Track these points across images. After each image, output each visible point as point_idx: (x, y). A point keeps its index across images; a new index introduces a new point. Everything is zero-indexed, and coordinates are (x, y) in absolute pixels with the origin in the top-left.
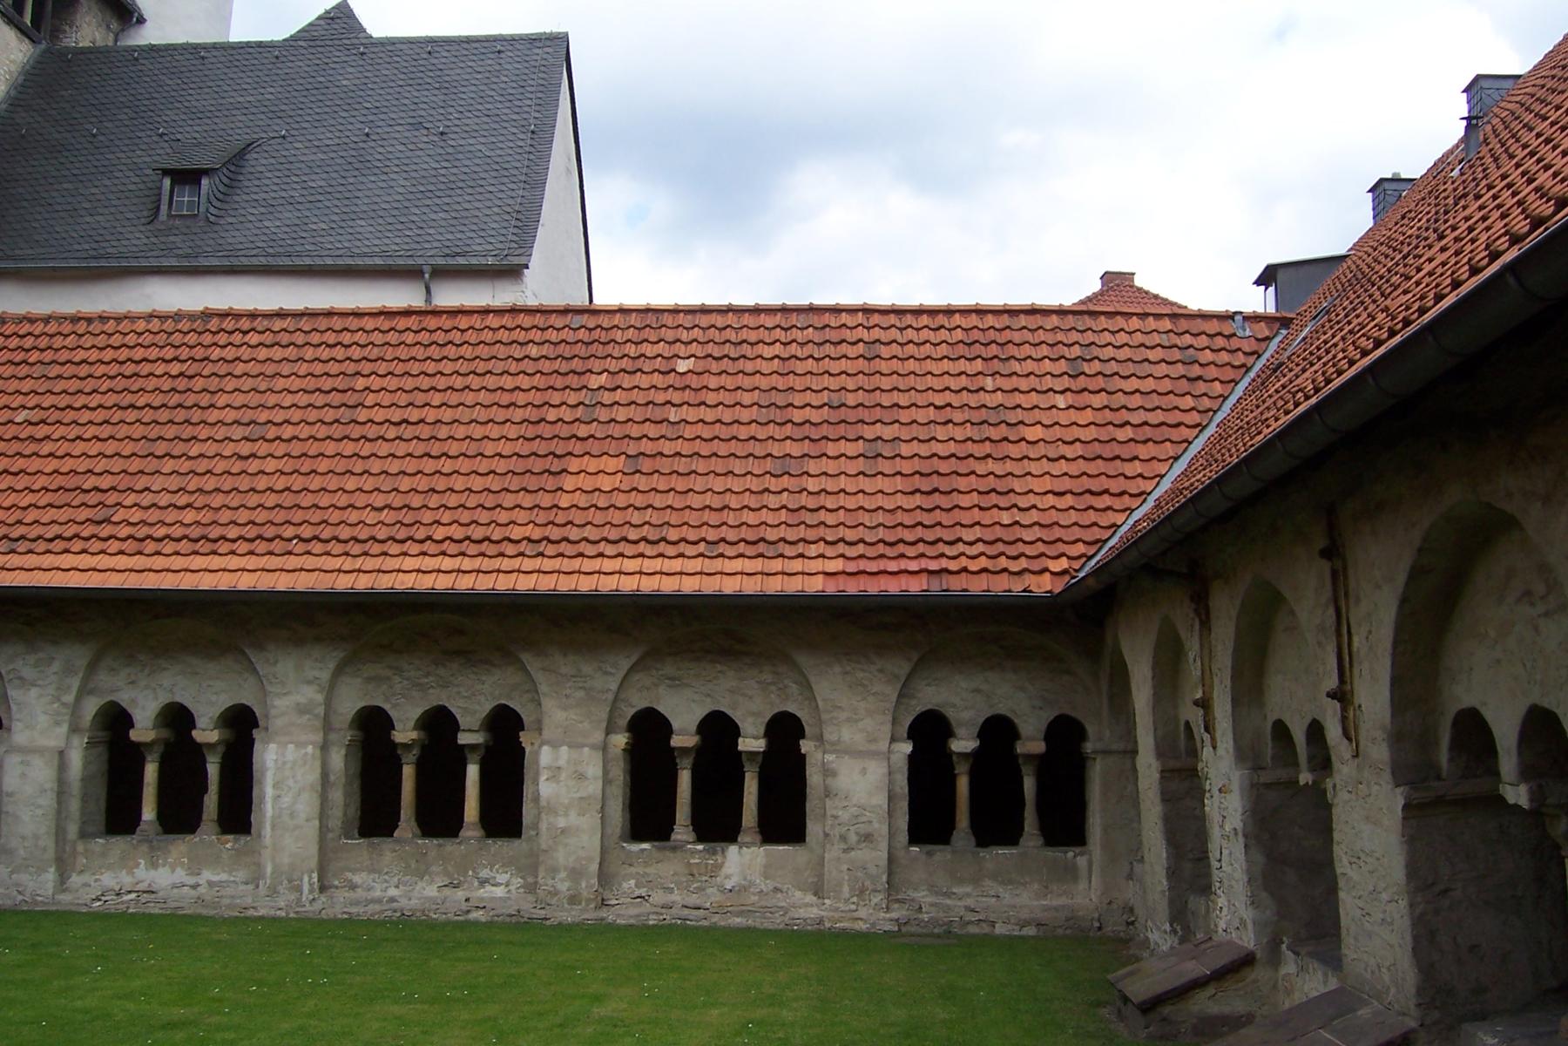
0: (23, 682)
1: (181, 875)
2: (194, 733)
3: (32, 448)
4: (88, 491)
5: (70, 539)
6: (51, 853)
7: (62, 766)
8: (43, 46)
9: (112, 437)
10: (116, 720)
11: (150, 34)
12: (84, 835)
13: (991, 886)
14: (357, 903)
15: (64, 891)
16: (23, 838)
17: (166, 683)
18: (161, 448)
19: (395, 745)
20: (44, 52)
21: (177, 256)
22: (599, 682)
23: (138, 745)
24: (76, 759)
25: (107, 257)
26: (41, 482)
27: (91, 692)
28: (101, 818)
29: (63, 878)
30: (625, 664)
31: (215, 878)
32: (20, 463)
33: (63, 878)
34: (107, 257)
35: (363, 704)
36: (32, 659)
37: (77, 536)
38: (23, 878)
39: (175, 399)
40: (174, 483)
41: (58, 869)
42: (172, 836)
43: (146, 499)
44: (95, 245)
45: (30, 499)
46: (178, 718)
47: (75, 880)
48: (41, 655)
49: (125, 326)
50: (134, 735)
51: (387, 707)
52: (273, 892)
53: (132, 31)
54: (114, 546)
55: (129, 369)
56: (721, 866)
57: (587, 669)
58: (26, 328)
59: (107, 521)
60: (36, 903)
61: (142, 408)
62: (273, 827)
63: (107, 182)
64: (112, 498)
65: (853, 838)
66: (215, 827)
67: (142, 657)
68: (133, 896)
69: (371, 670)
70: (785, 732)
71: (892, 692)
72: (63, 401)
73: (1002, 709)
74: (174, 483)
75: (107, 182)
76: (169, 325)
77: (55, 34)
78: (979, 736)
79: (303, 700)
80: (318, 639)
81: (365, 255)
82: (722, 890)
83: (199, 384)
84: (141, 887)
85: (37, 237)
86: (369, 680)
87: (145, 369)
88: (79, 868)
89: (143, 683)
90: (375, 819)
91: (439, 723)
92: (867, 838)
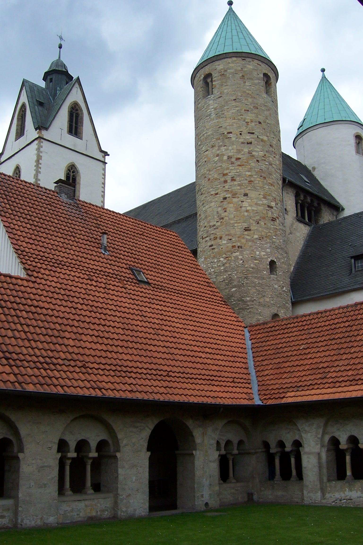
0: (306, 432)
2: (359, 445)
3: (305, 356)
4: (321, 368)
5: (358, 380)
6: (319, 486)
7: (320, 458)
8: (313, 226)
9: (328, 350)
10: (335, 442)
11: (347, 213)
12: (329, 480)
15: (324, 499)
16: (310, 482)
18: (342, 351)
20: (313, 228)
21: (359, 284)
23: (273, 454)
24: (324, 455)
25: (338, 288)
26: (307, 367)
27: (327, 433)
28: (335, 475)
29: (323, 495)
32: (302, 362)
33: (323, 495)
34: (338, 288)
37: (316, 384)
38: (311, 495)
39: (347, 334)
40: (346, 362)
41: (321, 492)
42: (356, 480)
43: (337, 369)
44: (334, 286)
45: (304, 373)
47: (327, 495)
49: (332, 313)
50: (341, 447)
53: (341, 214)
54: (327, 385)
55: (334, 326)
58: (304, 318)
59: (325, 377)
60: (315, 503)
61: (337, 339)
63: (336, 265)
64: (327, 370)
66: (70, 493)
68: (345, 501)
72: (315, 340)
74: (346, 362)
75: (336, 265)
76: (345, 310)
77: (316, 221)
78: (148, 450)
83: (354, 328)
84: (348, 497)
85: (317, 287)
87: (338, 326)
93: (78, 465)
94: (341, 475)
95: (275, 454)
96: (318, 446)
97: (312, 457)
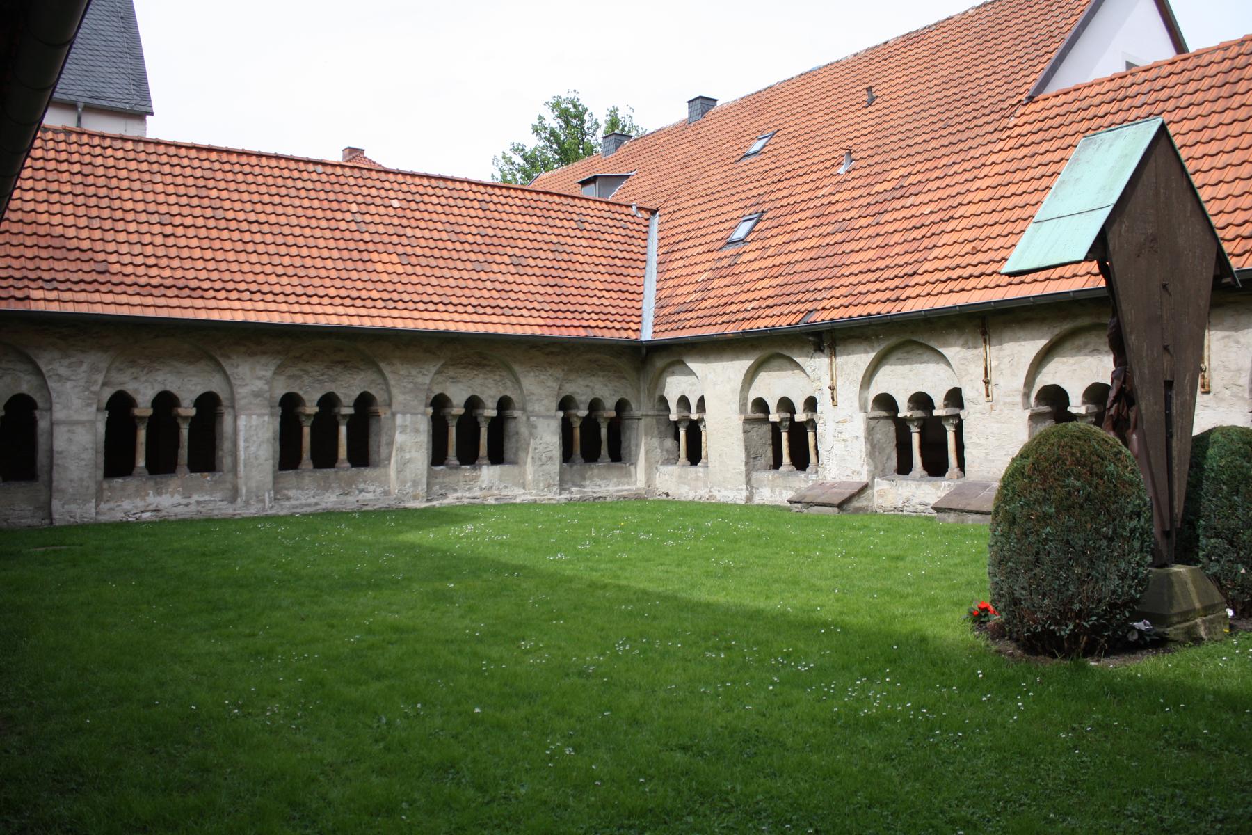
0: (60, 378)
1: (178, 498)
10: (886, 402)
14: (297, 507)
16: (71, 481)
17: (159, 379)
22: (420, 379)
25: (105, 99)
30: (434, 370)
31: (201, 499)
35: (284, 392)
36: (66, 362)
38: (73, 507)
46: (166, 402)
48: (73, 360)
51: (301, 393)
52: (247, 504)
57: (414, 372)
62: (245, 465)
66: (486, 461)
67: (142, 362)
69: (294, 371)
70: (365, 402)
71: (555, 385)
73: (598, 395)
80: (264, 353)
82: (481, 489)
84: (151, 508)
86: (290, 377)
88: (105, 498)
89: (143, 379)
90: (904, 467)
91: (329, 402)
93: (590, 424)
94: (904, 467)
95: (142, 418)
96: (89, 409)
97: (80, 430)
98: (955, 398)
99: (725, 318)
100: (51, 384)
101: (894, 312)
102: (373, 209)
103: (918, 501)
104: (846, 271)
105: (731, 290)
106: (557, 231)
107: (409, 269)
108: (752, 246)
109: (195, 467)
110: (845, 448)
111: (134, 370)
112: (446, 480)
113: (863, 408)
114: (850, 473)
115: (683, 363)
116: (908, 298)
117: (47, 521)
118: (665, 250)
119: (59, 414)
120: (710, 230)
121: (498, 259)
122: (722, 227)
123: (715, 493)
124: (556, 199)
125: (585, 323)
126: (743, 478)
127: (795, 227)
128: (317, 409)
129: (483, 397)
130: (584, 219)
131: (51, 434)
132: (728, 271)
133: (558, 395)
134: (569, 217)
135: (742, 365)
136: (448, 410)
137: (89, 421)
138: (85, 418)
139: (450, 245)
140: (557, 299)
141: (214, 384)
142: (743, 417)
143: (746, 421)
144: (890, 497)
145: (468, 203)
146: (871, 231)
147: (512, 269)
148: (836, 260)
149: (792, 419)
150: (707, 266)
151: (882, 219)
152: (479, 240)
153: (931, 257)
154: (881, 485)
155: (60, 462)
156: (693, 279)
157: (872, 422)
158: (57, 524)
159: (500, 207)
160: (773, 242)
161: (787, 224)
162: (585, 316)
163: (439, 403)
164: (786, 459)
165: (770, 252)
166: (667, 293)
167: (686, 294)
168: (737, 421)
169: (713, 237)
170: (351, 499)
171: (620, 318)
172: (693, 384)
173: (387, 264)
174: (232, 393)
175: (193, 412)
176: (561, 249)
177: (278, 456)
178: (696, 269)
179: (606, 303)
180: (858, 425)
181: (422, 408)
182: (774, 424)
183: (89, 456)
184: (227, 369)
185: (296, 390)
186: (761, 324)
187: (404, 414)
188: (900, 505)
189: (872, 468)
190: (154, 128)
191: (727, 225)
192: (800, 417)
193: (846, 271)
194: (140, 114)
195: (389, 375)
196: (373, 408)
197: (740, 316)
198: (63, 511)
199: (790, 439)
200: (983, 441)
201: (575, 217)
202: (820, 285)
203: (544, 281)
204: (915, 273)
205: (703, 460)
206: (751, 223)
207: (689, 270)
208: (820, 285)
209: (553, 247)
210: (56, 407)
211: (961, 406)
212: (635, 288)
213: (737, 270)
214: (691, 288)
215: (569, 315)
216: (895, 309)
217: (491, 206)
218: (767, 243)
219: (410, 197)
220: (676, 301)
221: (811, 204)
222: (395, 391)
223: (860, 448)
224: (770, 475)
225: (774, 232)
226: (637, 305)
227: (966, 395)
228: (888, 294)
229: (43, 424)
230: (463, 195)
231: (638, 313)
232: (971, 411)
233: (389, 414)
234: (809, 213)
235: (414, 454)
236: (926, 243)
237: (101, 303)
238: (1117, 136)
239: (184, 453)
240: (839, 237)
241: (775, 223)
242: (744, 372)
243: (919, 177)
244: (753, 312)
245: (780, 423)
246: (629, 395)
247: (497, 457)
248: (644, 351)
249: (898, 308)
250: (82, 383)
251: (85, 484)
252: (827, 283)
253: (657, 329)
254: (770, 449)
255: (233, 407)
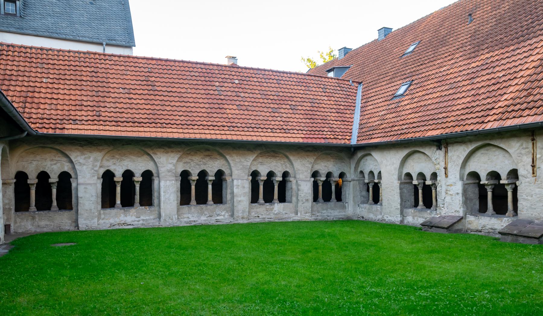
1: (134, 218)
10: (475, 175)
13: (330, 211)
16: (87, 210)
19: (133, 181)
22: (245, 164)
30: (252, 159)
31: (144, 218)
36: (83, 157)
50: (115, 179)
51: (190, 170)
56: (273, 208)
57: (243, 160)
62: (164, 203)
65: (304, 200)
66: (277, 201)
67: (117, 156)
69: (187, 160)
70: (220, 174)
71: (310, 166)
79: (168, 168)
80: (172, 152)
81: (82, 37)
82: (274, 214)
86: (185, 163)
92: (307, 200)
93: (327, 184)
94: (483, 209)
95: (118, 182)
96: (94, 178)
97: (89, 187)
98: (514, 174)
99: (392, 133)
100: (77, 167)
101: (481, 129)
102: (226, 85)
103: (490, 227)
104: (454, 108)
105: (395, 120)
106: (313, 93)
107: (242, 112)
108: (407, 97)
109: (141, 204)
110: (451, 199)
111: (113, 160)
112: (258, 210)
113: (461, 178)
114: (453, 211)
115: (370, 155)
116: (489, 121)
117: (76, 228)
118: (364, 101)
119: (80, 180)
120: (386, 91)
121: (284, 106)
122: (392, 89)
123: (385, 218)
124: (313, 78)
125: (324, 136)
126: (399, 211)
127: (429, 87)
128: (198, 178)
129: (275, 172)
130: (326, 87)
131: (77, 189)
132: (395, 110)
133: (311, 170)
134: (319, 86)
135: (403, 153)
136: (259, 178)
137: (94, 184)
138: (92, 182)
139: (261, 101)
140: (311, 125)
141: (150, 166)
142: (400, 182)
143: (401, 183)
144: (475, 224)
145: (271, 81)
146: (469, 87)
147: (291, 111)
148: (449, 103)
149: (424, 183)
150: (384, 108)
151: (475, 81)
152: (276, 98)
153: (503, 99)
154: (471, 218)
155: (81, 202)
156: (377, 114)
157: (466, 186)
158: (80, 229)
159: (286, 83)
160: (417, 95)
161: (424, 86)
162: (325, 133)
163: (255, 174)
164: (421, 203)
165: (416, 100)
166: (365, 121)
167: (374, 122)
168: (397, 184)
169: (388, 94)
170: (214, 218)
171: (341, 134)
172: (376, 166)
173: (231, 110)
174: (158, 170)
175: (141, 179)
176: (315, 101)
177: (179, 199)
178: (379, 110)
179: (335, 126)
180: (458, 187)
181: (246, 177)
182: (415, 185)
183: (93, 199)
184: (155, 159)
185: (188, 169)
186: (409, 136)
187: (238, 179)
188: (480, 228)
189: (465, 209)
190: (137, 52)
191: (394, 88)
192: (428, 182)
193: (454, 108)
194: (130, 44)
195: (231, 162)
196: (224, 177)
197: (399, 132)
198: (84, 224)
199: (423, 193)
200: (529, 198)
201: (322, 86)
202: (440, 116)
203: (306, 116)
204: (493, 108)
205: (380, 202)
206: (407, 86)
207: (376, 110)
208: (440, 116)
209: (311, 101)
210: (79, 177)
211: (517, 178)
212: (350, 120)
213: (398, 109)
214: (376, 119)
215: (317, 133)
216: (481, 127)
217: (282, 82)
218: (414, 96)
219: (244, 78)
220: (368, 125)
221: (437, 75)
222: (234, 169)
223: (459, 199)
224: (411, 211)
225: (418, 90)
226: (350, 127)
227: (521, 172)
228: (478, 120)
229: (74, 185)
230: (269, 77)
231: (350, 131)
232: (523, 182)
233: (231, 180)
234: (436, 80)
235: (242, 198)
236: (500, 92)
237: (72, 129)
238: (459, 122)
239: (137, 197)
240: (451, 92)
241: (418, 86)
242: (401, 160)
243: (497, 58)
244: (406, 130)
245: (418, 185)
246: (345, 170)
247: (282, 199)
248: (352, 149)
249: (483, 127)
250: (90, 166)
251: (92, 211)
252: (444, 115)
253: (359, 139)
254: (413, 197)
255: (158, 177)
